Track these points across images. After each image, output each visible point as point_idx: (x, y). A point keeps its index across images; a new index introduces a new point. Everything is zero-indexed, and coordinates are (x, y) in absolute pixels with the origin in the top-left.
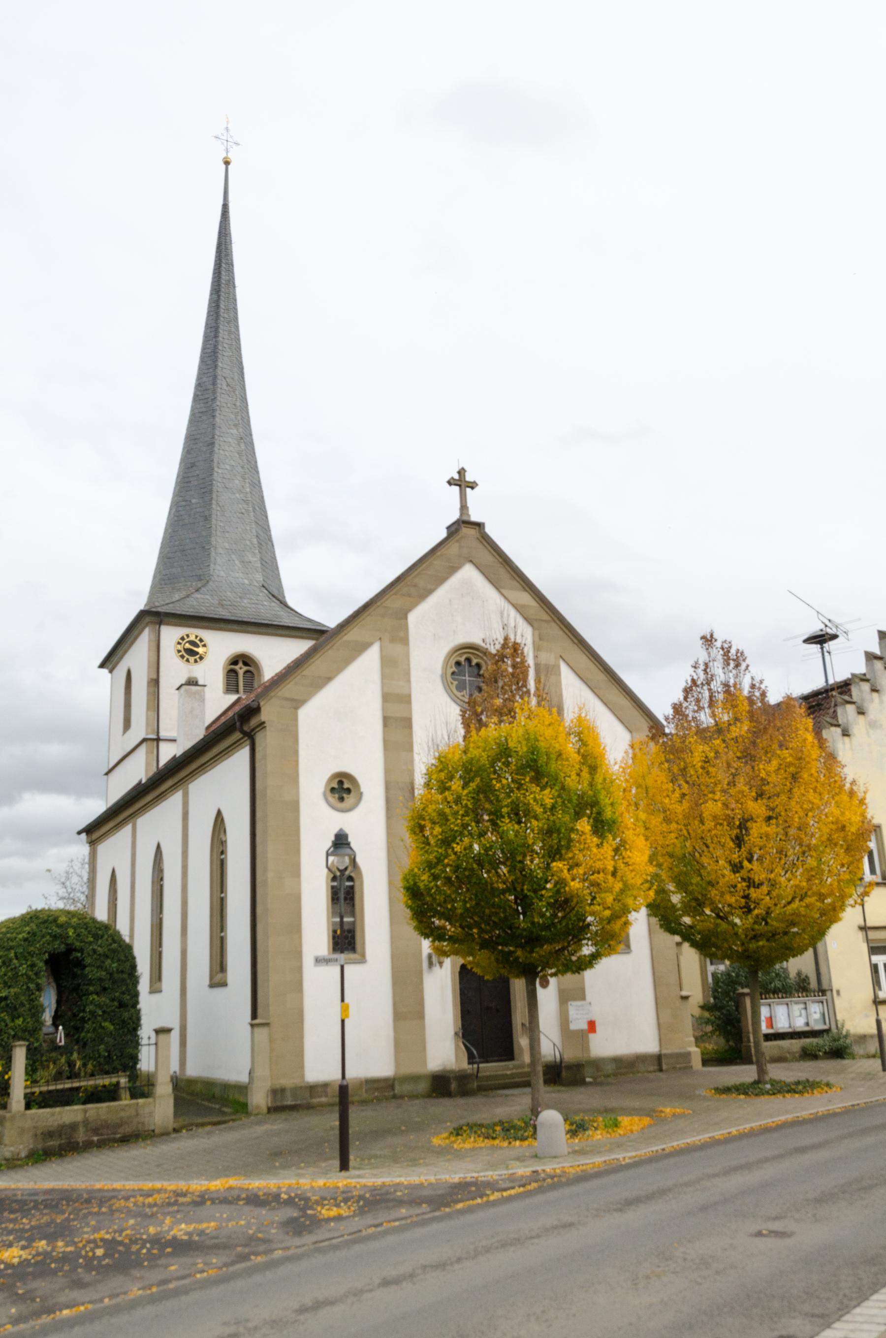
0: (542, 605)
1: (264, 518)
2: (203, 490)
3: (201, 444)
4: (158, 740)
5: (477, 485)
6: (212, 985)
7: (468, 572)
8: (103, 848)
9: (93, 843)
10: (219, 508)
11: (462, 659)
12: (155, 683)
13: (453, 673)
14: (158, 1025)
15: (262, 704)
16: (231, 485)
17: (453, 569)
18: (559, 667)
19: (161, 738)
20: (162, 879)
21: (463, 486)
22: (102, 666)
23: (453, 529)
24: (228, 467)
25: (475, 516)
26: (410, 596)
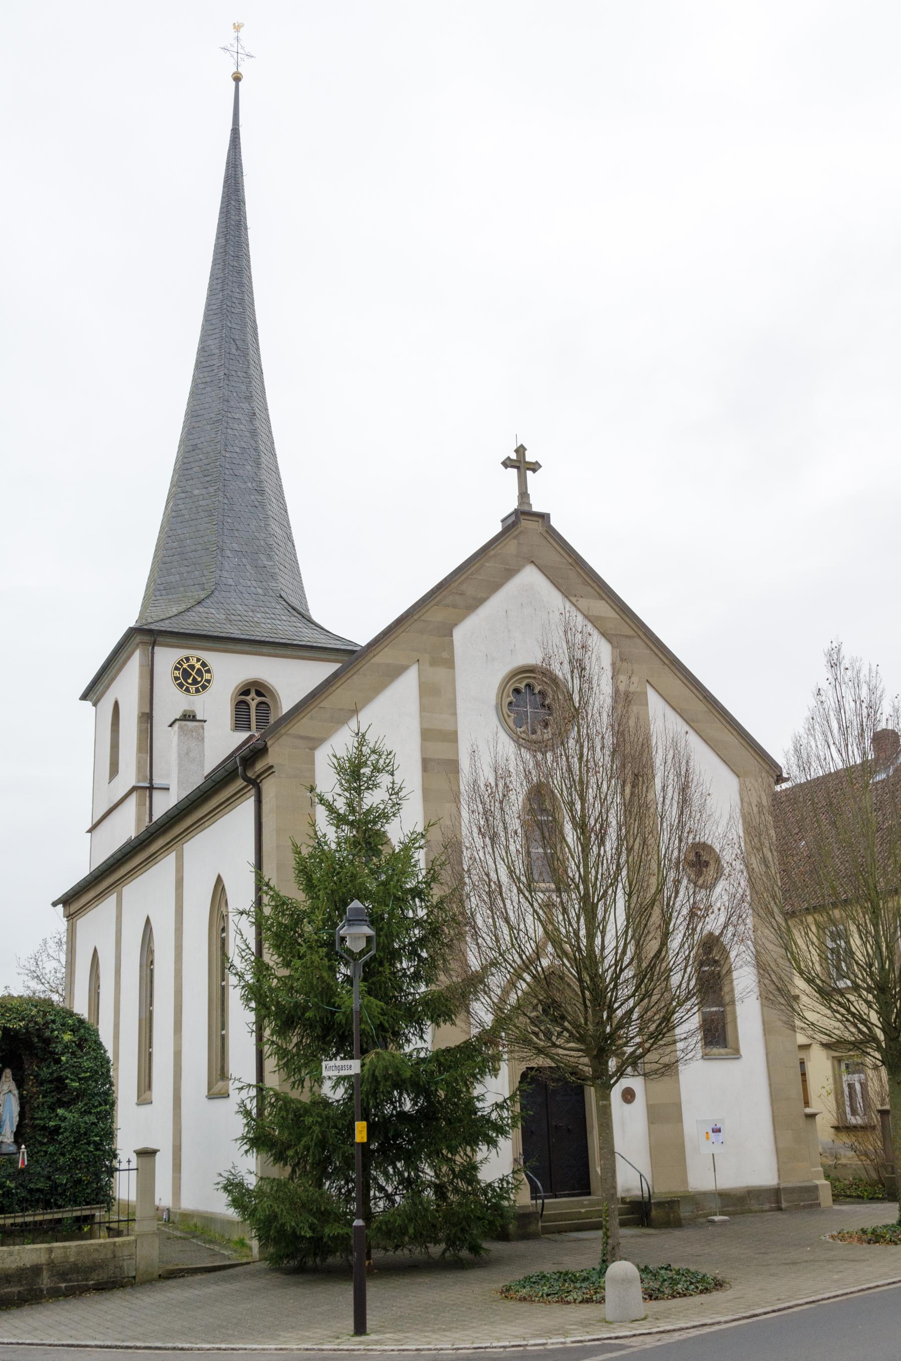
0: (624, 616)
1: (283, 512)
2: (208, 479)
3: (205, 422)
4: (151, 788)
5: (540, 466)
6: (211, 1096)
7: (530, 576)
8: (82, 923)
9: (71, 917)
10: (226, 501)
11: (522, 686)
12: (147, 718)
13: (510, 703)
14: (140, 1146)
15: (269, 743)
16: (241, 471)
17: (510, 573)
18: (645, 694)
19: (155, 786)
20: (152, 963)
21: (522, 469)
22: (84, 697)
23: (510, 521)
24: (238, 450)
25: (537, 507)
26: (455, 606)
